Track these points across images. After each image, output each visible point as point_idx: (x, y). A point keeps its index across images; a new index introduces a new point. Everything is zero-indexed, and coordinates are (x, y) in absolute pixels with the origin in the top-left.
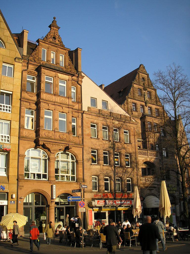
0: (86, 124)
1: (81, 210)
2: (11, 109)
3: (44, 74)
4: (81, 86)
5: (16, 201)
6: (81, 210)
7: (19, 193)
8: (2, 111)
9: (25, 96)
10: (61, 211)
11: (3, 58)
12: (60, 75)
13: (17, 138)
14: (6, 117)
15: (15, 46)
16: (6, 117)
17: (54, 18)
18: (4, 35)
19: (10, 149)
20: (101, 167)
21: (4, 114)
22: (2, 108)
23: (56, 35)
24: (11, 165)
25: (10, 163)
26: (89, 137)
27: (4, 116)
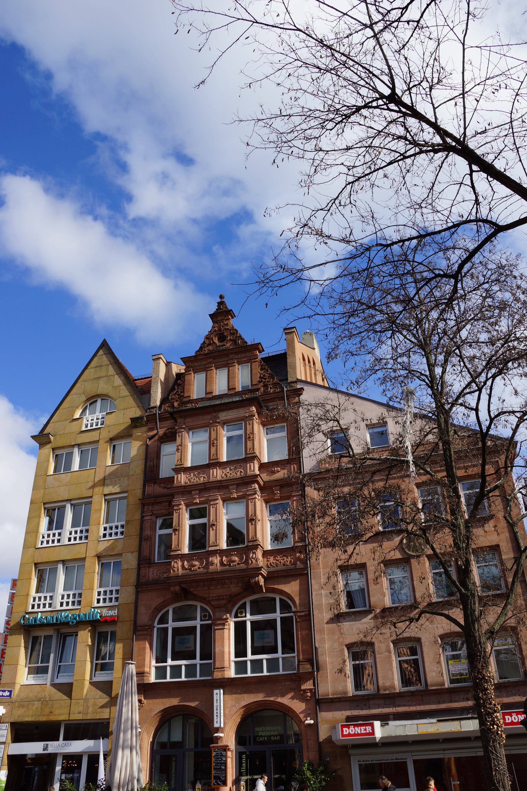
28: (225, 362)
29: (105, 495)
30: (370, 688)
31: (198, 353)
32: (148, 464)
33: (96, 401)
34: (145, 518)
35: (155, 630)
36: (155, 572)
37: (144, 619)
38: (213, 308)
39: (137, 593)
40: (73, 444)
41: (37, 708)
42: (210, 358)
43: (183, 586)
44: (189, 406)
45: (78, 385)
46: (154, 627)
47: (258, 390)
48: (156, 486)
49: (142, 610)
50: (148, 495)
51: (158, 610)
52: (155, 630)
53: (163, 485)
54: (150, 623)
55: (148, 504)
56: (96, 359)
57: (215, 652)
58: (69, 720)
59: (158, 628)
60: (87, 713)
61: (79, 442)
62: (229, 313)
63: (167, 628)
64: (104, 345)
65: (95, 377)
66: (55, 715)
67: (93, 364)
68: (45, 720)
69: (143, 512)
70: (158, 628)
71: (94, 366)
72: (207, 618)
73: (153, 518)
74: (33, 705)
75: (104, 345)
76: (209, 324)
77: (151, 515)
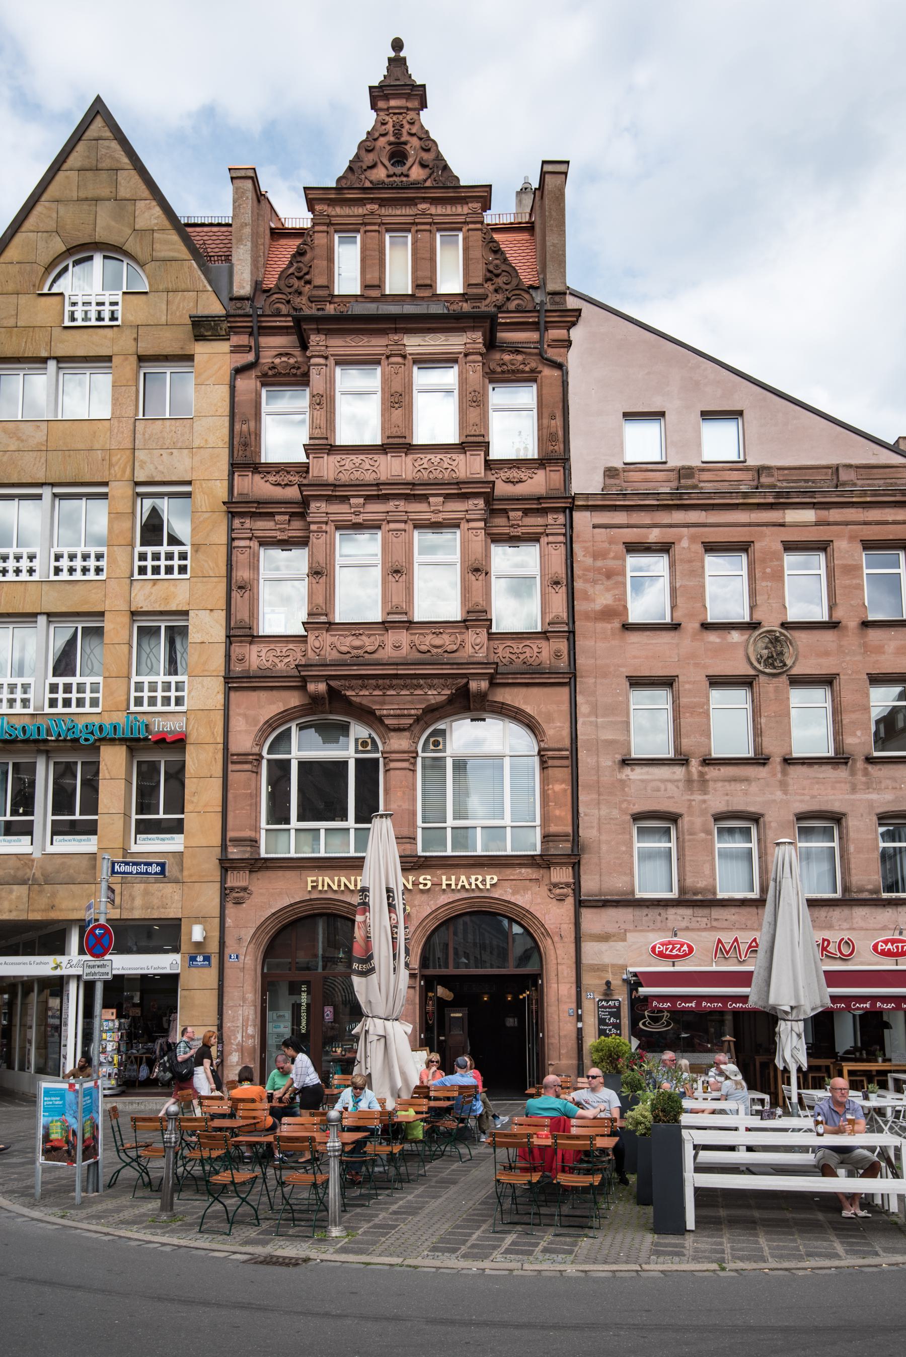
0: (589, 561)
1: (93, 970)
2: (137, 563)
3: (322, 361)
4: (560, 366)
5: (217, 955)
6: (93, 970)
7: (229, 922)
8: (11, 576)
9: (254, 489)
10: (510, 993)
11: (136, 340)
12: (414, 344)
13: (217, 685)
14: (166, 600)
15: (190, 267)
16: (166, 600)
17: (397, 45)
18: (137, 227)
19: (181, 733)
20: (689, 773)
21: (156, 587)
22: (11, 564)
23: (405, 138)
24: (192, 802)
25: (186, 797)
26: (609, 626)
27: (153, 598)
28: (409, 220)
29: (137, 484)
30: (228, 843)
31: (343, 184)
32: (237, 427)
33: (90, 258)
34: (236, 543)
35: (264, 763)
36: (263, 654)
37: (243, 742)
38: (377, 74)
39: (228, 690)
40: (44, 354)
41: (18, 898)
42: (372, 200)
43: (332, 683)
44: (330, 309)
45: (39, 208)
46: (262, 757)
47: (484, 297)
48: (257, 477)
49: (238, 724)
50: (240, 494)
51: (271, 725)
52: (264, 763)
53: (272, 478)
54: (256, 750)
55: (242, 515)
56: (81, 147)
57: (129, 782)
58: (120, 920)
59: (269, 761)
60: (132, 909)
61: (61, 350)
62: (418, 95)
63: (289, 761)
64: (230, 169)
65: (82, 195)
66: (61, 910)
67: (74, 160)
68: (39, 918)
69: (231, 530)
70: (269, 761)
71: (78, 164)
72: (369, 748)
73: (254, 544)
74: (11, 892)
75: (230, 169)
76: (368, 119)
77: (250, 539)
